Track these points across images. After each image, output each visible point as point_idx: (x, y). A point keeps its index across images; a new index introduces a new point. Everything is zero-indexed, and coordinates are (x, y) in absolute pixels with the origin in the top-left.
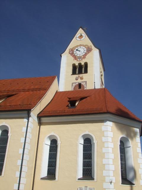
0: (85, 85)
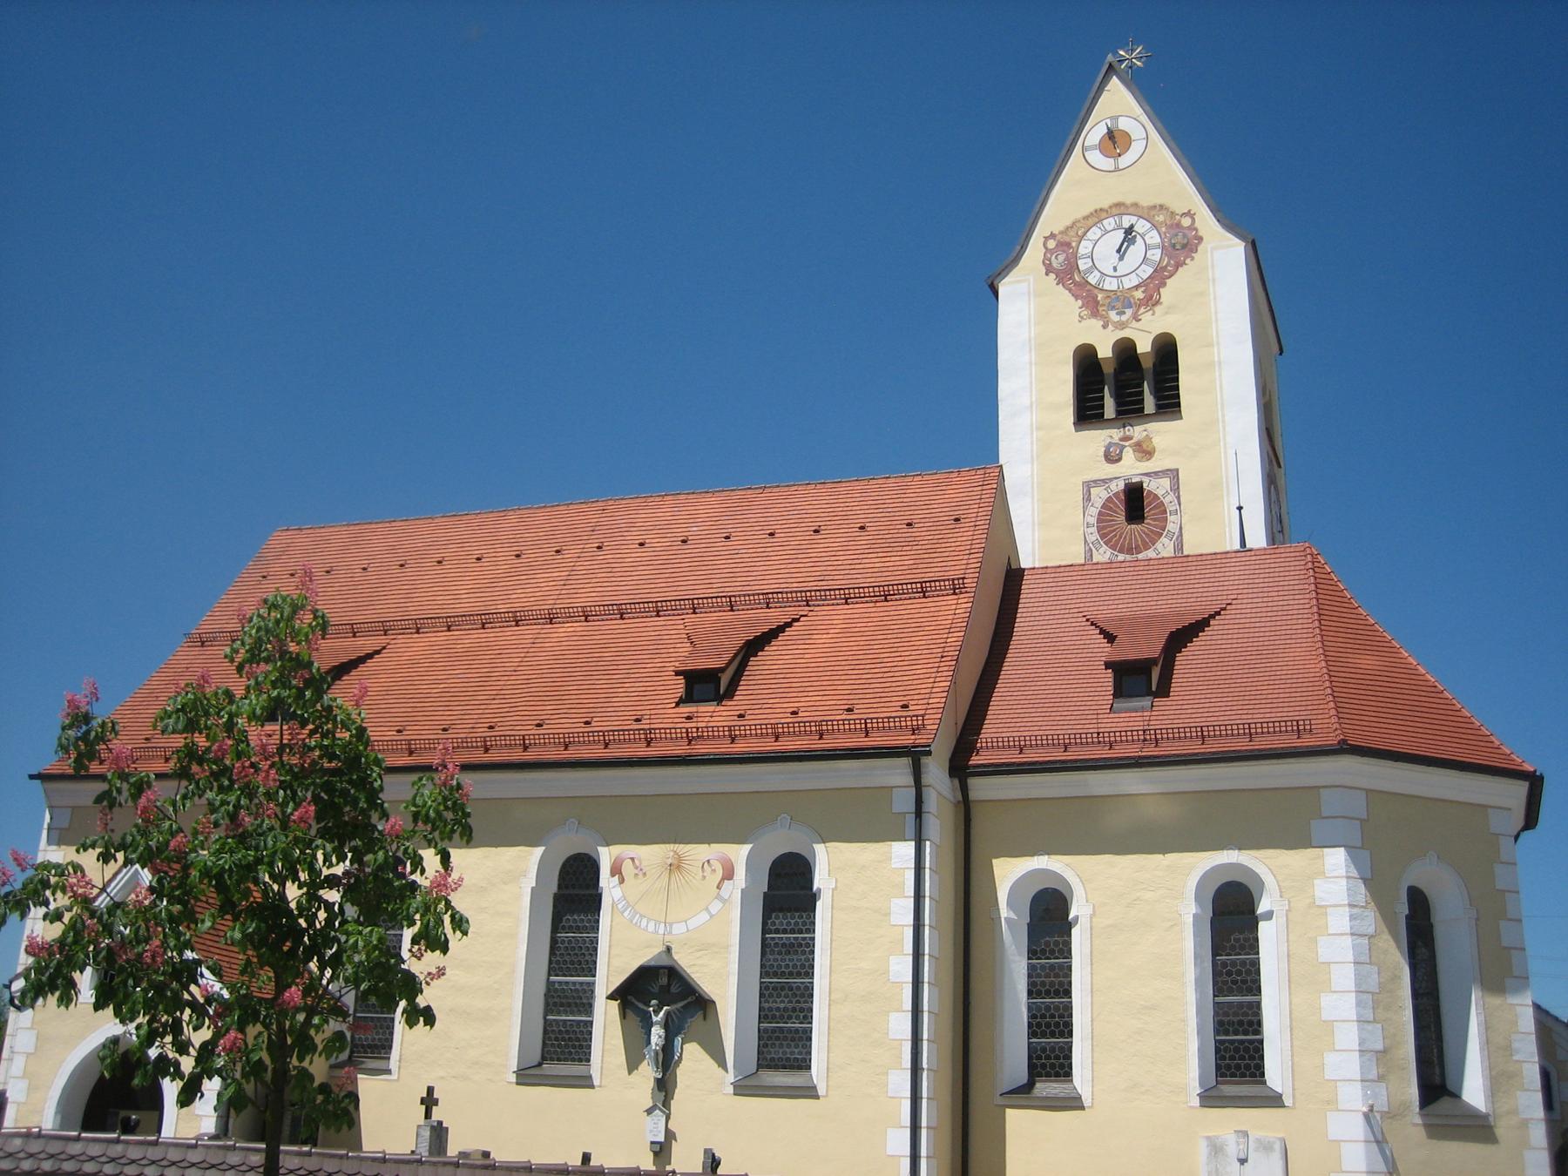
0: (1171, 497)
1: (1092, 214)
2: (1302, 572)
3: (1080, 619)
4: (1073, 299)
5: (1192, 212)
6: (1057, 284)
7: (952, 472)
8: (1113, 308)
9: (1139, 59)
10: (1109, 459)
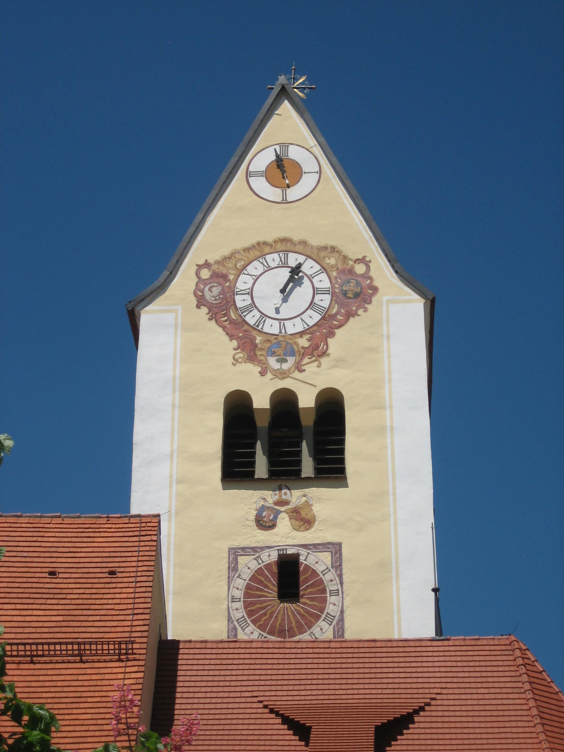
1: (253, 246)
2: (512, 668)
3: (255, 705)
4: (226, 338)
5: (367, 259)
6: (210, 319)
7: (100, 517)
8: (273, 354)
9: (302, 89)
10: (261, 525)
